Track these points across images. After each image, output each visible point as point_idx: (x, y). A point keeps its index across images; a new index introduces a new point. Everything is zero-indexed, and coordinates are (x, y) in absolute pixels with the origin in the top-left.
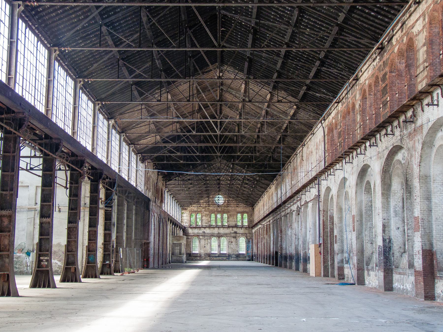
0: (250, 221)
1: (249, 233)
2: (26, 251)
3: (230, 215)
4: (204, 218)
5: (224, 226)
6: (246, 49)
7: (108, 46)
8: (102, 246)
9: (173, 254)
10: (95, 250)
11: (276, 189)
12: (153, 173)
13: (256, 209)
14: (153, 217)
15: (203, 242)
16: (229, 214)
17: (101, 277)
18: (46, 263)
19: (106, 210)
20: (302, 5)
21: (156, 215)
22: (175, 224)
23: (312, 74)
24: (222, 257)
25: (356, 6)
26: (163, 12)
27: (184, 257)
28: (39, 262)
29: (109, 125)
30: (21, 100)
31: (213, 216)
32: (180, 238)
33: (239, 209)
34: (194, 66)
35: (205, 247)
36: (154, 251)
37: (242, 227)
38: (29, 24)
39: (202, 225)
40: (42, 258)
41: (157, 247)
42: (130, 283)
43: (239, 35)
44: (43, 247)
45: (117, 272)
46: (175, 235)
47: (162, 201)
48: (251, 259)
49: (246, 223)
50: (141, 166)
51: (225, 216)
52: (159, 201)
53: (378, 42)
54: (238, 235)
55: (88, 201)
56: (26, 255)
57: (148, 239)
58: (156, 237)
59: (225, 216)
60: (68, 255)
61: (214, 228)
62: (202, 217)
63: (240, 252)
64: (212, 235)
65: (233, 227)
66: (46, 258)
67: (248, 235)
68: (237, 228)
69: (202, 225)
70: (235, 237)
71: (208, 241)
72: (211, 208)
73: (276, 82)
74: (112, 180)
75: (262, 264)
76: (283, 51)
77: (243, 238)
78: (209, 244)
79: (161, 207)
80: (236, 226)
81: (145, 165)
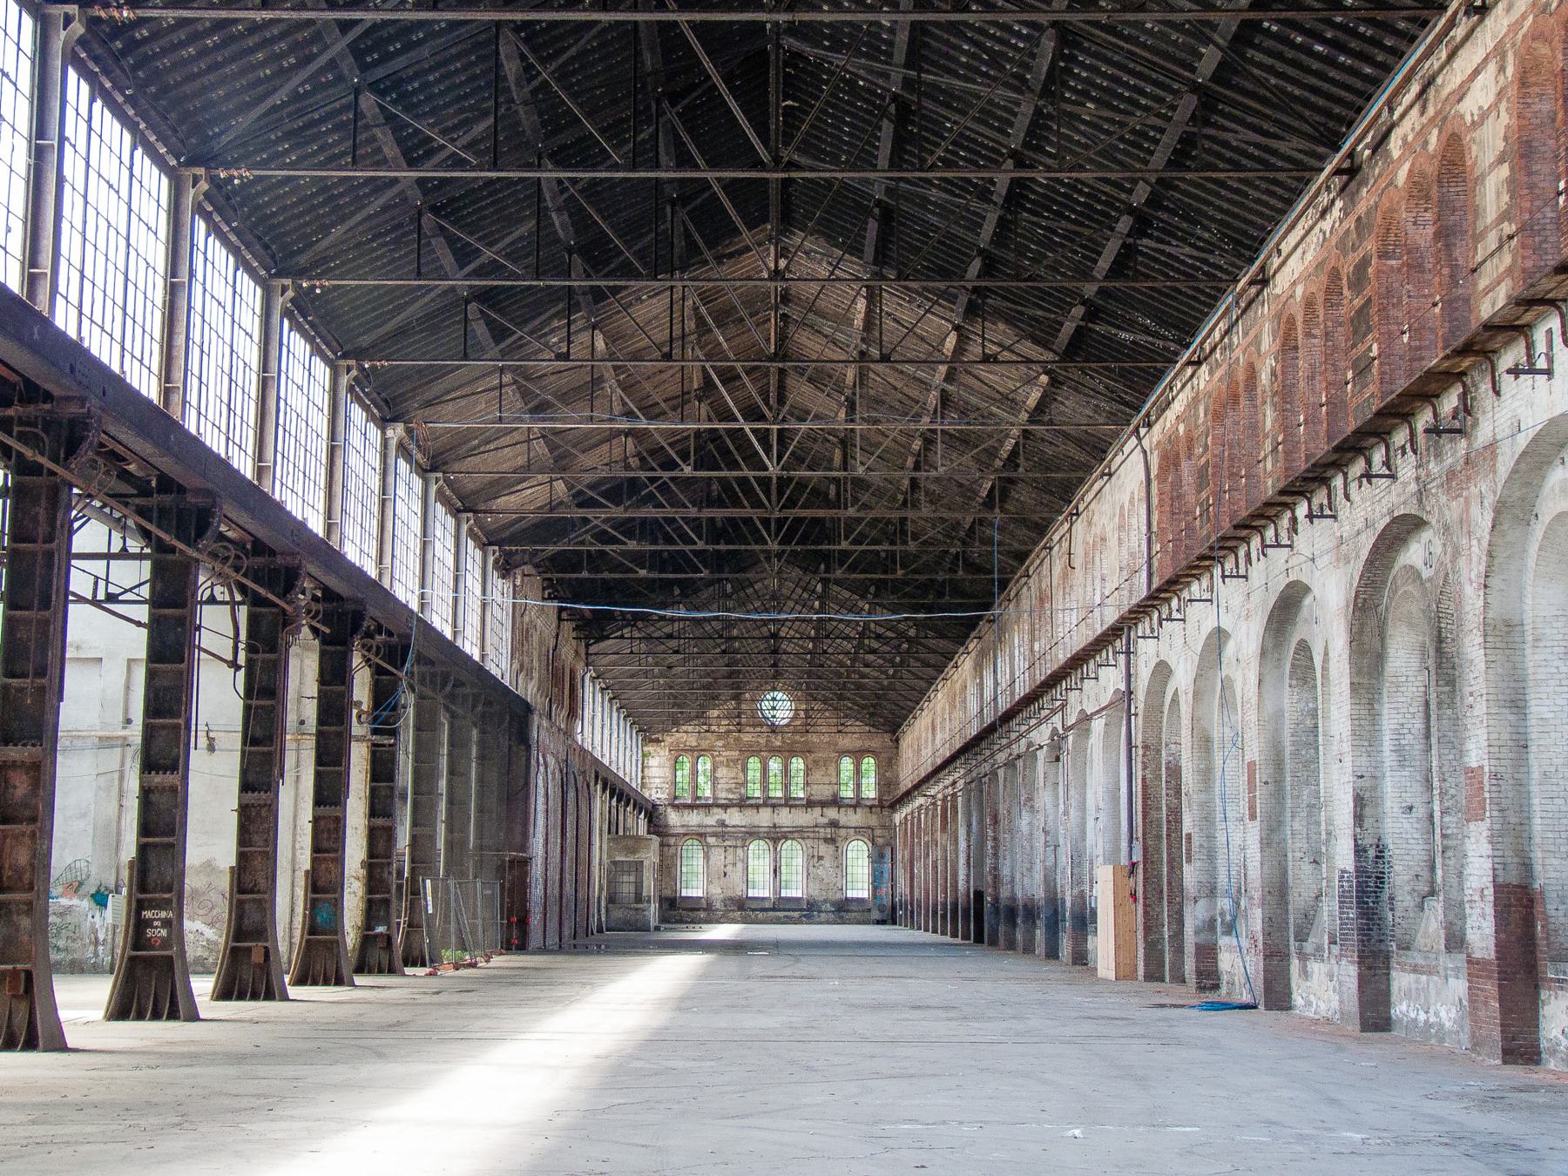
0: (885, 784)
1: (883, 827)
2: (93, 891)
3: (816, 762)
4: (722, 772)
5: (791, 802)
6: (872, 175)
7: (382, 163)
8: (362, 872)
9: (612, 900)
10: (337, 887)
11: (978, 668)
12: (543, 613)
13: (908, 740)
14: (542, 769)
15: (718, 856)
16: (811, 757)
17: (359, 980)
18: (164, 933)
19: (374, 745)
20: (1067, 17)
21: (551, 760)
22: (620, 793)
23: (1104, 263)
24: (784, 910)
25: (1261, 21)
26: (576, 41)
27: (653, 912)
28: (138, 928)
29: (385, 443)
30: (73, 355)
31: (754, 764)
32: (635, 843)
33: (845, 742)
34: (687, 235)
35: (725, 874)
36: (545, 889)
37: (857, 804)
38: (102, 86)
39: (715, 798)
40: (147, 914)
41: (554, 875)
42: (459, 1004)
43: (847, 124)
44: (152, 877)
45: (414, 965)
46: (621, 833)
47: (573, 713)
48: (890, 917)
49: (870, 791)
50: (500, 589)
51: (798, 764)
52: (564, 713)
53: (1338, 149)
54: (843, 832)
55: (310, 711)
56: (93, 904)
57: (524, 847)
58: (551, 839)
59: (798, 764)
60: (240, 903)
61: (757, 807)
62: (714, 770)
63: (850, 894)
64: (752, 834)
65: (823, 804)
66: (163, 914)
67: (878, 832)
68: (839, 807)
69: (715, 798)
70: (831, 841)
71: (735, 854)
72: (746, 738)
73: (975, 290)
74: (395, 639)
75: (929, 937)
76: (1002, 180)
77: (861, 843)
78: (740, 865)
79: (569, 733)
80: (836, 802)
81: (515, 586)
